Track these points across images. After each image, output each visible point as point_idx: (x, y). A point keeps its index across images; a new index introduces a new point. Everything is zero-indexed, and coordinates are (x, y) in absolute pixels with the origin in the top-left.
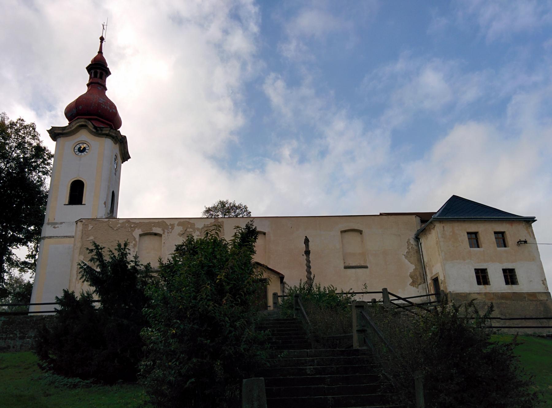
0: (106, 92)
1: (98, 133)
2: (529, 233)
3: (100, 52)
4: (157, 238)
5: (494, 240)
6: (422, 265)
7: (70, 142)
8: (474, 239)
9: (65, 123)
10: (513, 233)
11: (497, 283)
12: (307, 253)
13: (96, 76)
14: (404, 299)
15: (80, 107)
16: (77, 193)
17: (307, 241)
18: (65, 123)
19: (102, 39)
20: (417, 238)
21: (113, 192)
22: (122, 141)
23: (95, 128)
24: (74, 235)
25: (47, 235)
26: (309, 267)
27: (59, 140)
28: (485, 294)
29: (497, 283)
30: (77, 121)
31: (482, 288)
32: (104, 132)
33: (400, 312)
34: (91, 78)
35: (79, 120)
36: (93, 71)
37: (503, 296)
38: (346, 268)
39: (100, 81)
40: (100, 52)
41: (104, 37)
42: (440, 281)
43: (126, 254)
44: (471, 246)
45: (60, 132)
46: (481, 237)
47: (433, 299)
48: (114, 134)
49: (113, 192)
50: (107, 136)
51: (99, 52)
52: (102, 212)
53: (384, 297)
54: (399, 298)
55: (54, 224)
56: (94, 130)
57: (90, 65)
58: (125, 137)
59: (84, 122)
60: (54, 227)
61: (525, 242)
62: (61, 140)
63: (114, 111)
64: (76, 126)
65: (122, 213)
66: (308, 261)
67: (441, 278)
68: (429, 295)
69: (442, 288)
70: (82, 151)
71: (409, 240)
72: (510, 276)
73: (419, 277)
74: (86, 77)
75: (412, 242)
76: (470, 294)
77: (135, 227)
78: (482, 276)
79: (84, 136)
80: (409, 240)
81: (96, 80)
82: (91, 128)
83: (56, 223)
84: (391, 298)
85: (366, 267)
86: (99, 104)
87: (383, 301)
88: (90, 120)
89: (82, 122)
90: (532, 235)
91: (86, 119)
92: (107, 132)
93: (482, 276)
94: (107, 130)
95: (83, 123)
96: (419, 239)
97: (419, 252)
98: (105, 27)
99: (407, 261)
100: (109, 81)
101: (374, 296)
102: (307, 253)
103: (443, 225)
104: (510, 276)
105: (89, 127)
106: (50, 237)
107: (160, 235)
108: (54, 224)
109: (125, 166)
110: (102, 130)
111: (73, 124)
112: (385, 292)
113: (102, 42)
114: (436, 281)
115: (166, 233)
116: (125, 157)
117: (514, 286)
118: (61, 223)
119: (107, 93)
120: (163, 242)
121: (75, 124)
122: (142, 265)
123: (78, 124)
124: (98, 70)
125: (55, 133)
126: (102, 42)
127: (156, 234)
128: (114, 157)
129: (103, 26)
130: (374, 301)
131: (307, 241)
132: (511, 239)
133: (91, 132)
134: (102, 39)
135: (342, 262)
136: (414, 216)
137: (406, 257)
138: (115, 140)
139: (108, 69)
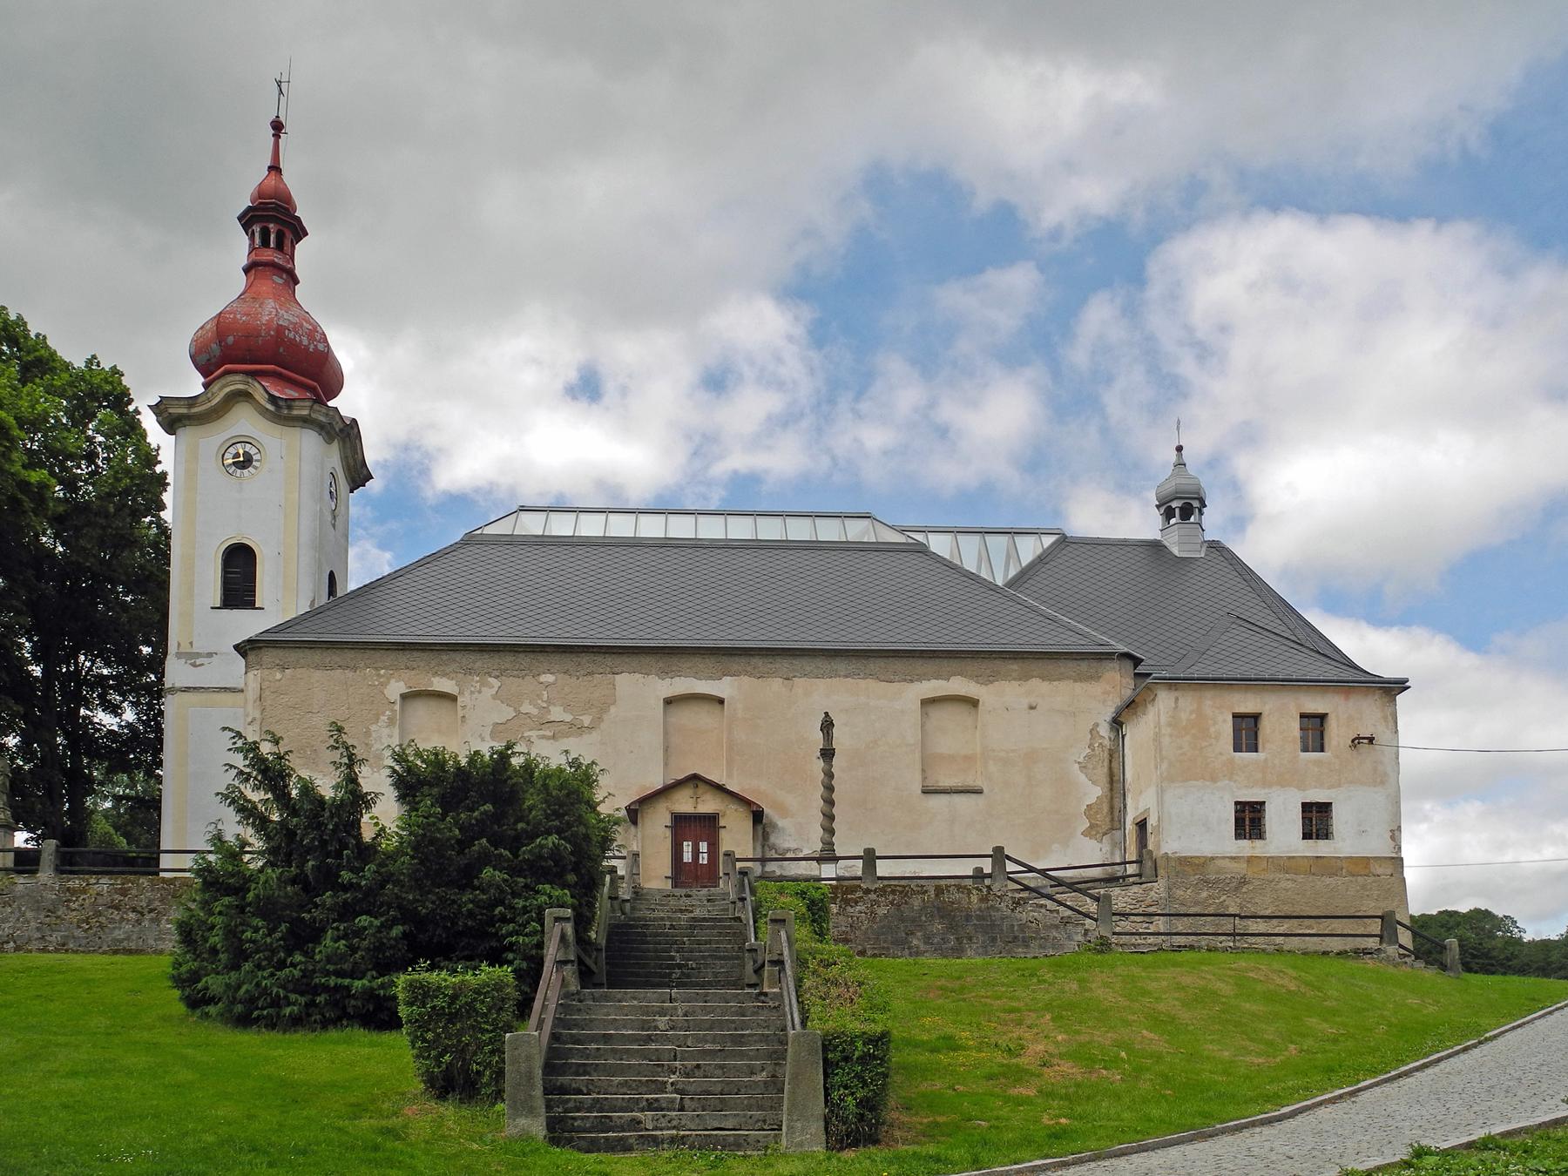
1: (280, 414)
2: (1385, 718)
3: (275, 168)
4: (447, 704)
5: (1297, 733)
6: (1116, 785)
7: (211, 439)
8: (1247, 731)
9: (192, 384)
10: (1346, 716)
11: (1284, 833)
12: (828, 754)
13: (265, 242)
14: (1043, 872)
15: (230, 340)
17: (827, 725)
20: (1117, 723)
23: (273, 399)
24: (242, 686)
25: (177, 685)
26: (829, 788)
27: (180, 431)
28: (1250, 860)
29: (1284, 833)
30: (223, 381)
31: (1246, 847)
32: (295, 412)
33: (1025, 901)
34: (252, 249)
35: (230, 378)
36: (257, 228)
37: (1287, 865)
39: (278, 258)
40: (275, 168)
41: (282, 119)
42: (1149, 829)
44: (1237, 748)
46: (1266, 726)
48: (322, 419)
49: (332, 575)
50: (306, 422)
51: (270, 168)
54: (1031, 869)
55: (192, 658)
56: (269, 407)
57: (249, 209)
59: (241, 382)
60: (194, 665)
61: (1371, 740)
62: (187, 433)
63: (321, 347)
64: (222, 394)
66: (829, 775)
67: (1152, 822)
70: (246, 462)
72: (1316, 819)
74: (240, 247)
75: (1104, 731)
76: (1213, 858)
78: (1250, 819)
79: (245, 423)
80: (1097, 725)
81: (270, 255)
82: (263, 402)
83: (198, 655)
84: (1011, 867)
85: (979, 792)
86: (280, 330)
88: (254, 374)
89: (236, 383)
90: (1391, 724)
92: (305, 412)
93: (1250, 819)
94: (302, 408)
96: (1121, 724)
97: (1115, 756)
98: (284, 86)
99: (1082, 777)
101: (977, 863)
102: (828, 754)
103: (1177, 694)
104: (1316, 819)
105: (257, 397)
106: (187, 689)
107: (453, 698)
110: (290, 408)
111: (215, 387)
112: (999, 855)
113: (277, 136)
114: (1142, 825)
115: (467, 694)
117: (1321, 842)
118: (210, 655)
120: (460, 713)
121: (221, 389)
123: (227, 390)
125: (173, 416)
126: (277, 136)
128: (328, 479)
129: (279, 84)
130: (979, 870)
131: (827, 725)
132: (1337, 734)
133: (263, 412)
134: (278, 127)
135: (918, 777)
137: (1083, 768)
138: (328, 433)
139: (298, 219)
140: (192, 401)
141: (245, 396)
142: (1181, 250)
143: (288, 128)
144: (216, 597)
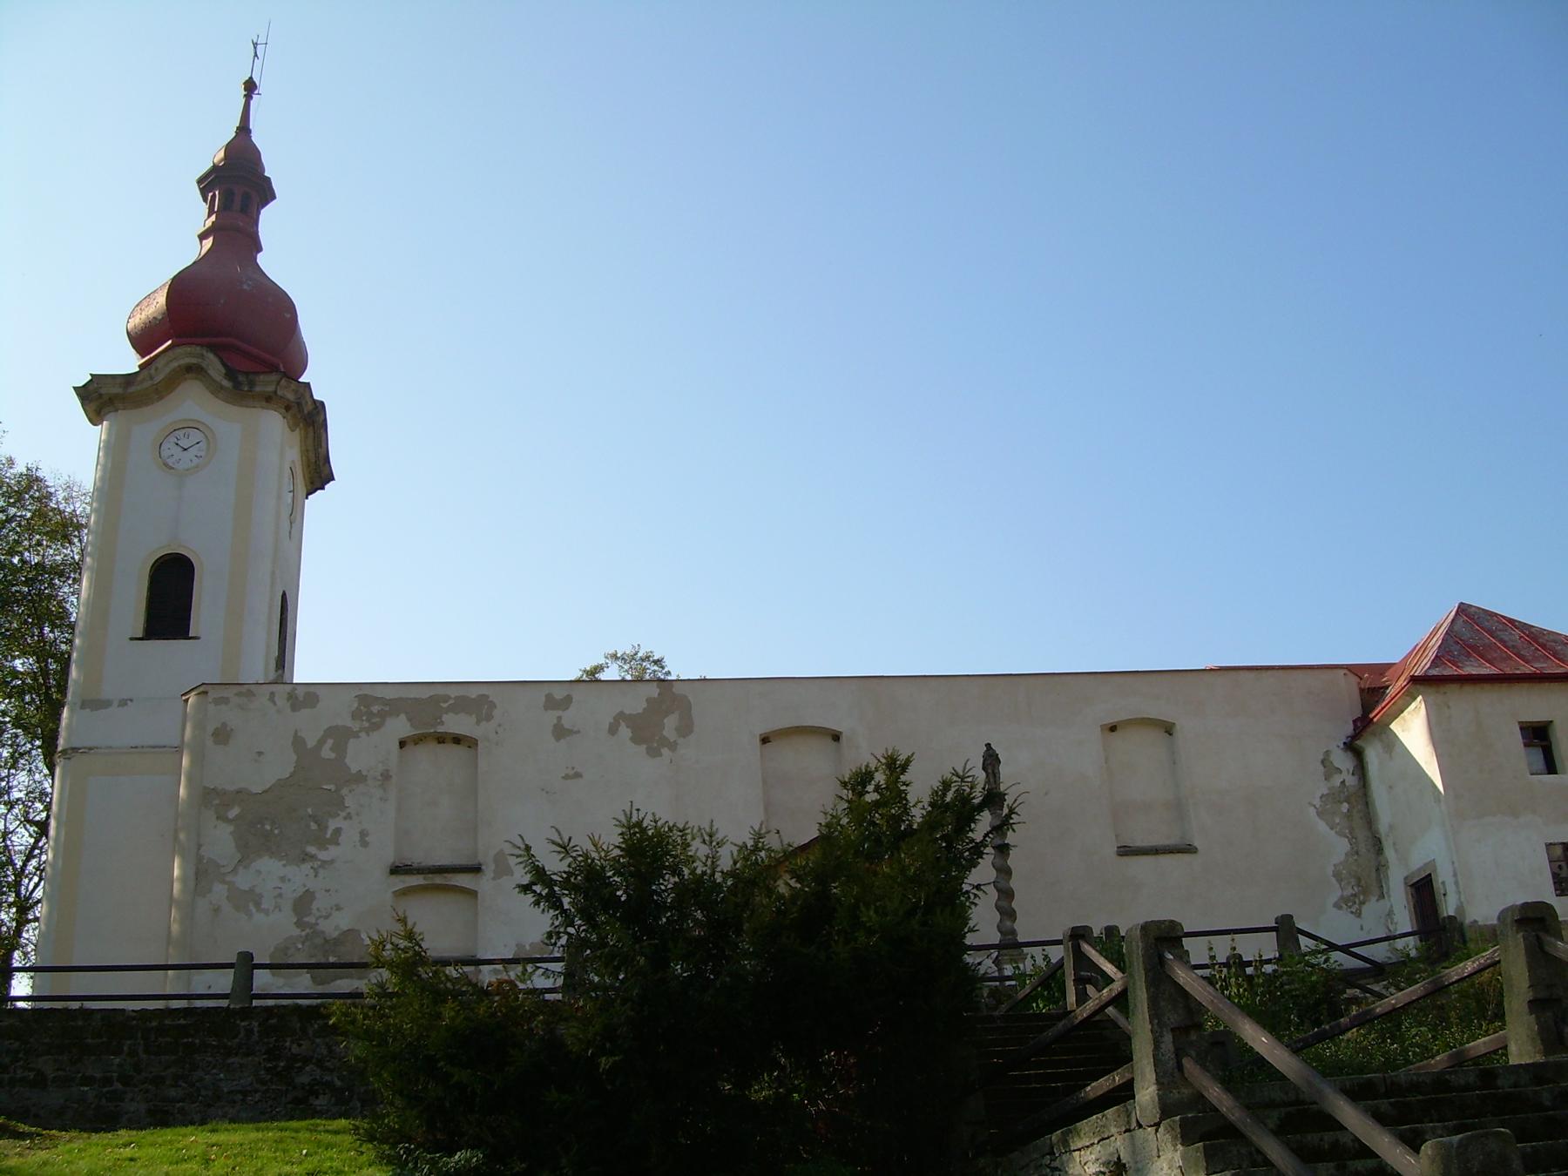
0: (259, 256)
3: (244, 129)
7: (149, 425)
9: (127, 362)
14: (1345, 949)
16: (170, 598)
18: (127, 362)
19: (250, 87)
21: (284, 594)
22: (310, 419)
23: (231, 374)
38: (1126, 851)
40: (244, 129)
43: (341, 804)
45: (117, 390)
47: (1411, 945)
49: (284, 594)
50: (269, 399)
52: (256, 668)
53: (1281, 944)
54: (1332, 947)
56: (226, 383)
57: (215, 168)
58: (322, 403)
59: (190, 355)
64: (168, 370)
65: (308, 668)
67: (1443, 877)
68: (1395, 938)
69: (1449, 908)
71: (1327, 753)
73: (1365, 878)
74: (198, 215)
75: (1344, 761)
77: (383, 715)
79: (193, 403)
80: (1327, 753)
85: (1189, 849)
87: (1279, 960)
89: (187, 355)
91: (201, 345)
92: (271, 388)
95: (188, 360)
100: (269, 221)
105: (211, 372)
108: (92, 704)
109: (316, 505)
113: (248, 97)
114: (1423, 890)
116: (318, 474)
118: (123, 703)
119: (262, 260)
122: (986, 835)
123: (175, 364)
124: (238, 185)
126: (248, 97)
127: (457, 740)
129: (255, 45)
133: (217, 390)
134: (250, 87)
136: (1342, 672)
140: (128, 379)
141: (194, 370)
142: (304, 440)
143: (261, 89)
144: (138, 625)
